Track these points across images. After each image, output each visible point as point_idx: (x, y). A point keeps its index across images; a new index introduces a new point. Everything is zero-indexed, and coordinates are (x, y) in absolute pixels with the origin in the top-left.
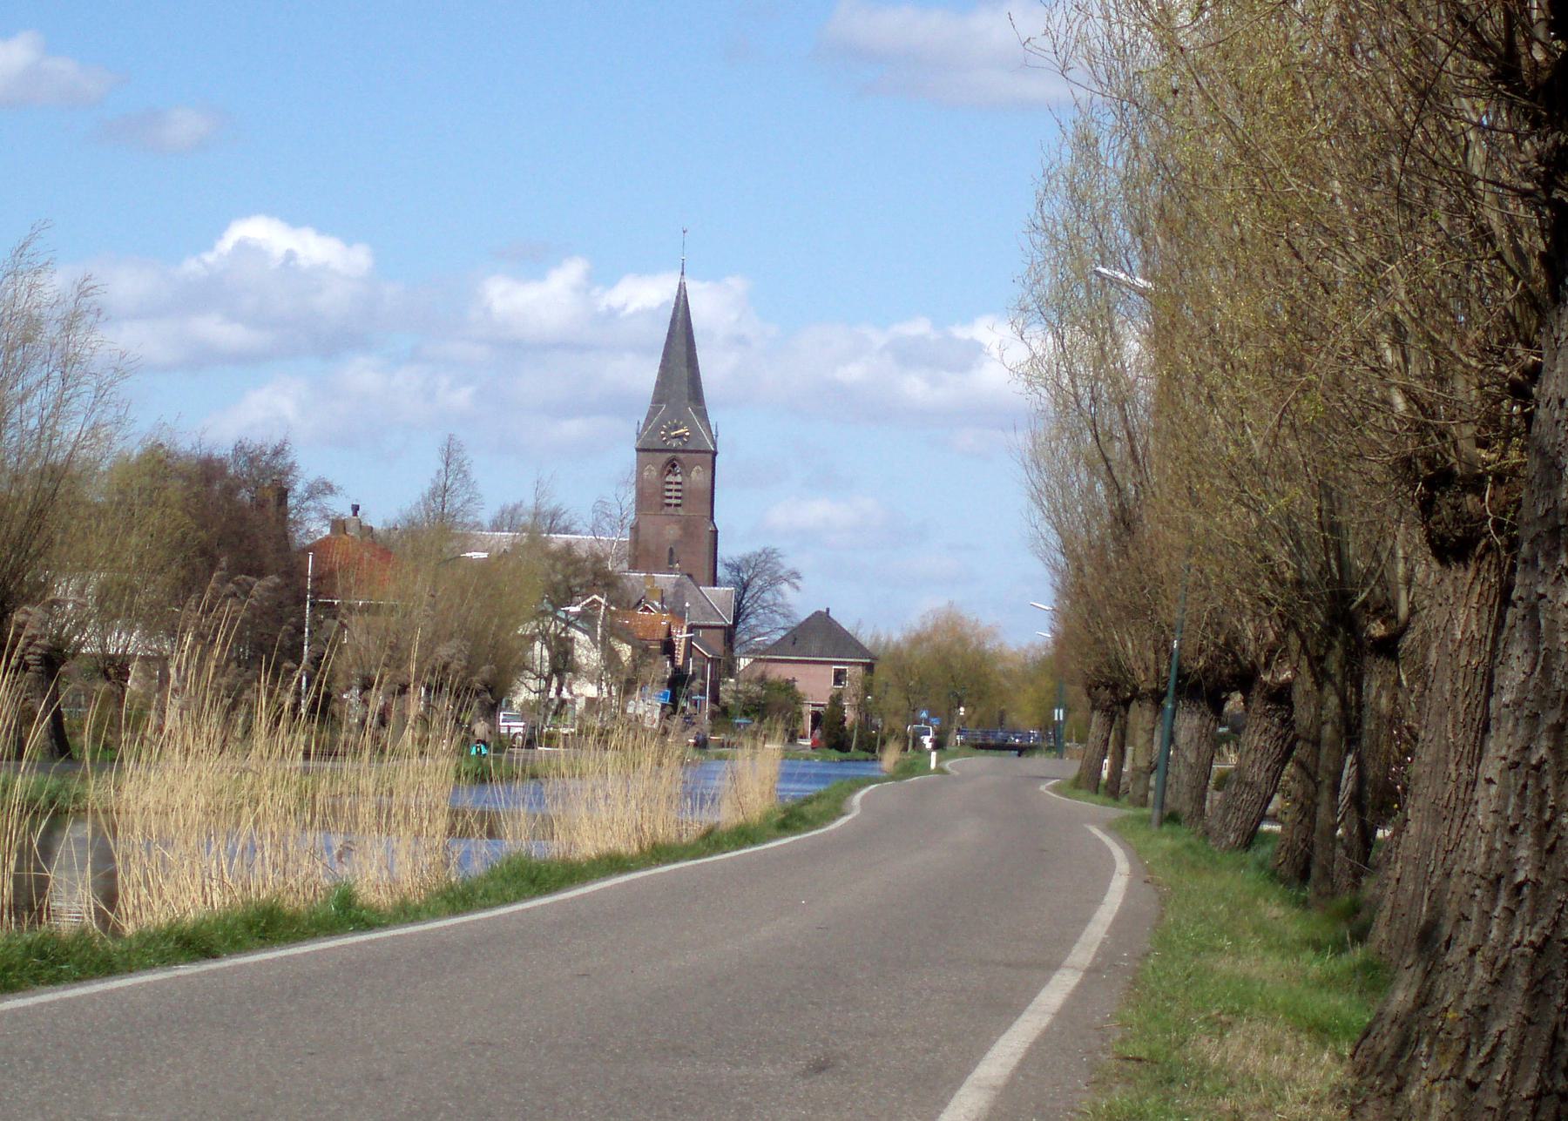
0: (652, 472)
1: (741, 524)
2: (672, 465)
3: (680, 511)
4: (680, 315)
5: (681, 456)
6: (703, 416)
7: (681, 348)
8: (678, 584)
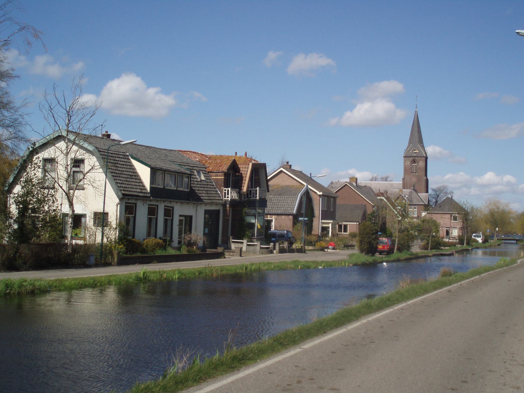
0: (408, 163)
1: (436, 179)
2: (414, 161)
3: (417, 174)
4: (416, 119)
5: (416, 158)
6: (423, 147)
7: (416, 128)
8: (410, 193)
